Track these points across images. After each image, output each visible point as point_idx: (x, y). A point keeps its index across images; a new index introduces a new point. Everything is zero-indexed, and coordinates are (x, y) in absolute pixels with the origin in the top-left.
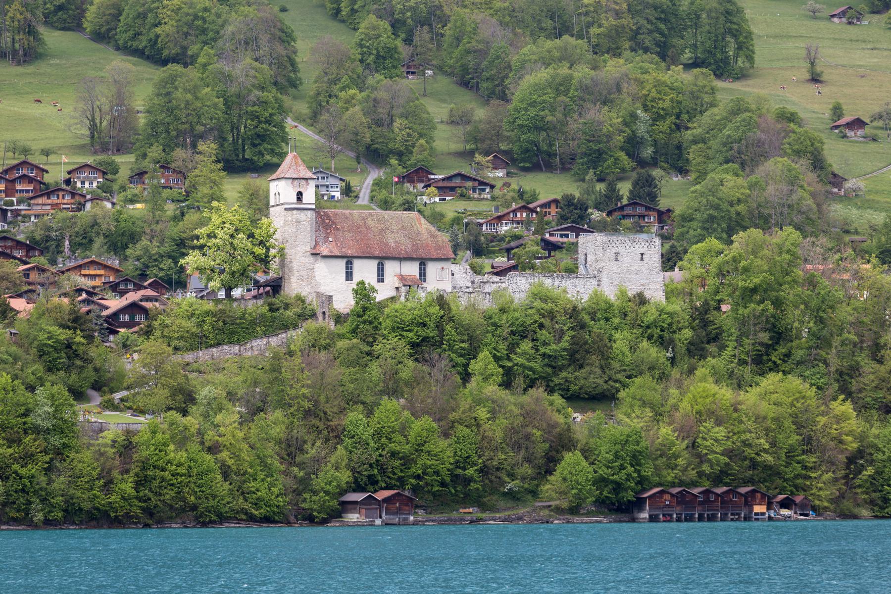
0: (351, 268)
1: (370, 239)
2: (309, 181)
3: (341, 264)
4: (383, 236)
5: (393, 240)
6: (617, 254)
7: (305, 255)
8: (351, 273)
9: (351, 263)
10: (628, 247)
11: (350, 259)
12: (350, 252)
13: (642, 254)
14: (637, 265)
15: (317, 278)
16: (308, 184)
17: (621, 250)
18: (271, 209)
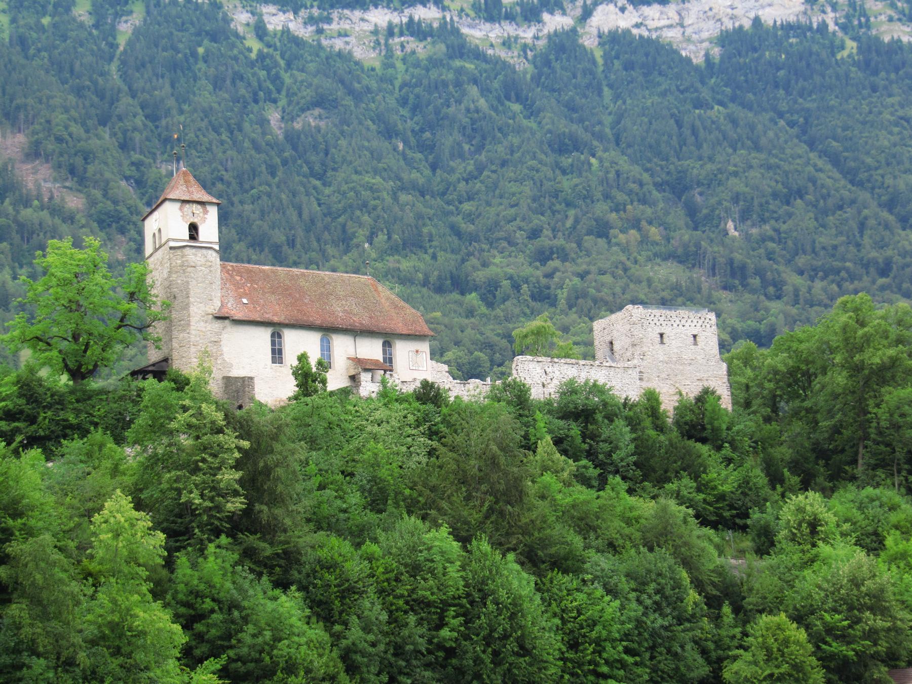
0: (280, 344)
1: (306, 304)
2: (209, 208)
3: (263, 336)
4: (325, 303)
5: (339, 311)
6: (661, 335)
7: (205, 319)
8: (280, 352)
9: (280, 336)
10: (675, 325)
11: (277, 329)
12: (276, 319)
13: (695, 336)
14: (690, 352)
15: (226, 357)
16: (206, 212)
17: (667, 330)
18: (149, 261)
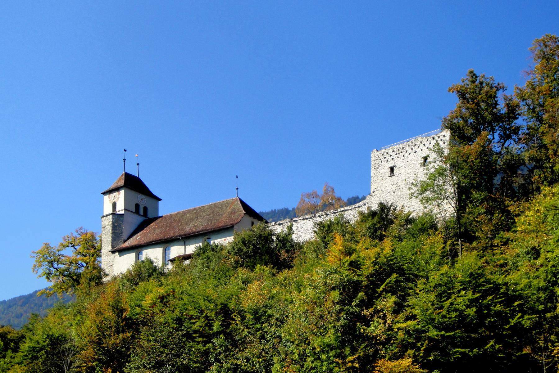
10: (406, 154)
